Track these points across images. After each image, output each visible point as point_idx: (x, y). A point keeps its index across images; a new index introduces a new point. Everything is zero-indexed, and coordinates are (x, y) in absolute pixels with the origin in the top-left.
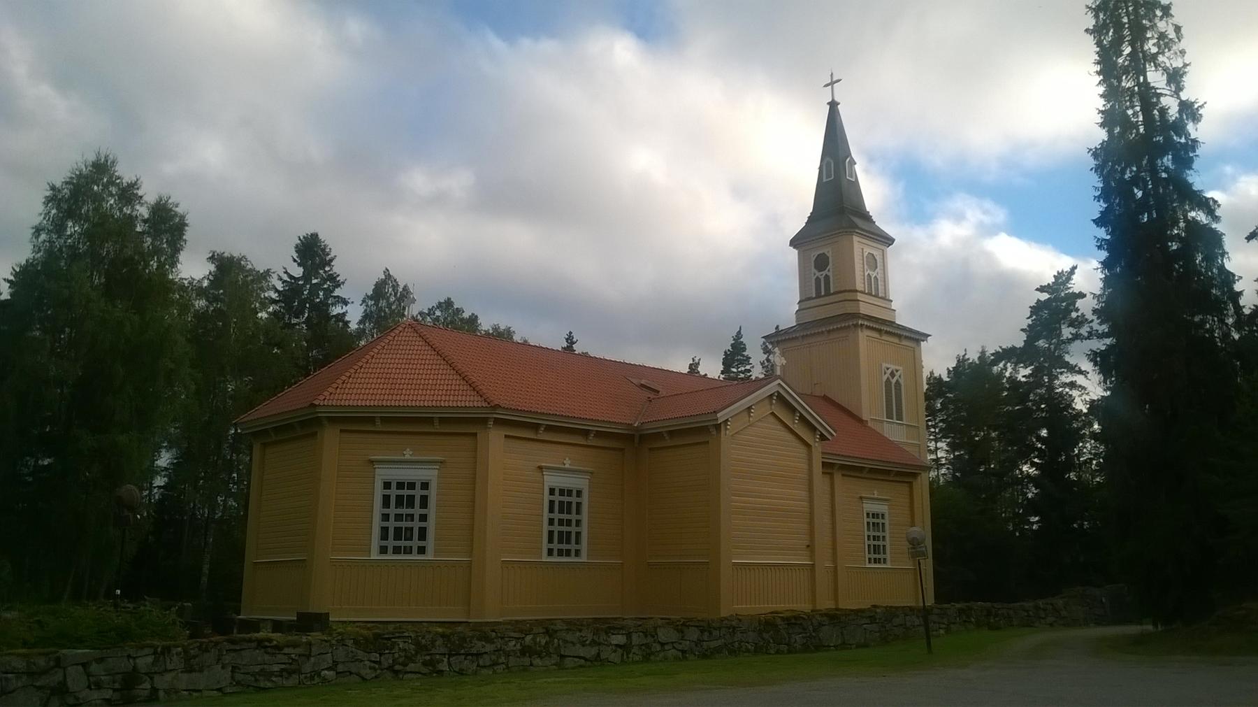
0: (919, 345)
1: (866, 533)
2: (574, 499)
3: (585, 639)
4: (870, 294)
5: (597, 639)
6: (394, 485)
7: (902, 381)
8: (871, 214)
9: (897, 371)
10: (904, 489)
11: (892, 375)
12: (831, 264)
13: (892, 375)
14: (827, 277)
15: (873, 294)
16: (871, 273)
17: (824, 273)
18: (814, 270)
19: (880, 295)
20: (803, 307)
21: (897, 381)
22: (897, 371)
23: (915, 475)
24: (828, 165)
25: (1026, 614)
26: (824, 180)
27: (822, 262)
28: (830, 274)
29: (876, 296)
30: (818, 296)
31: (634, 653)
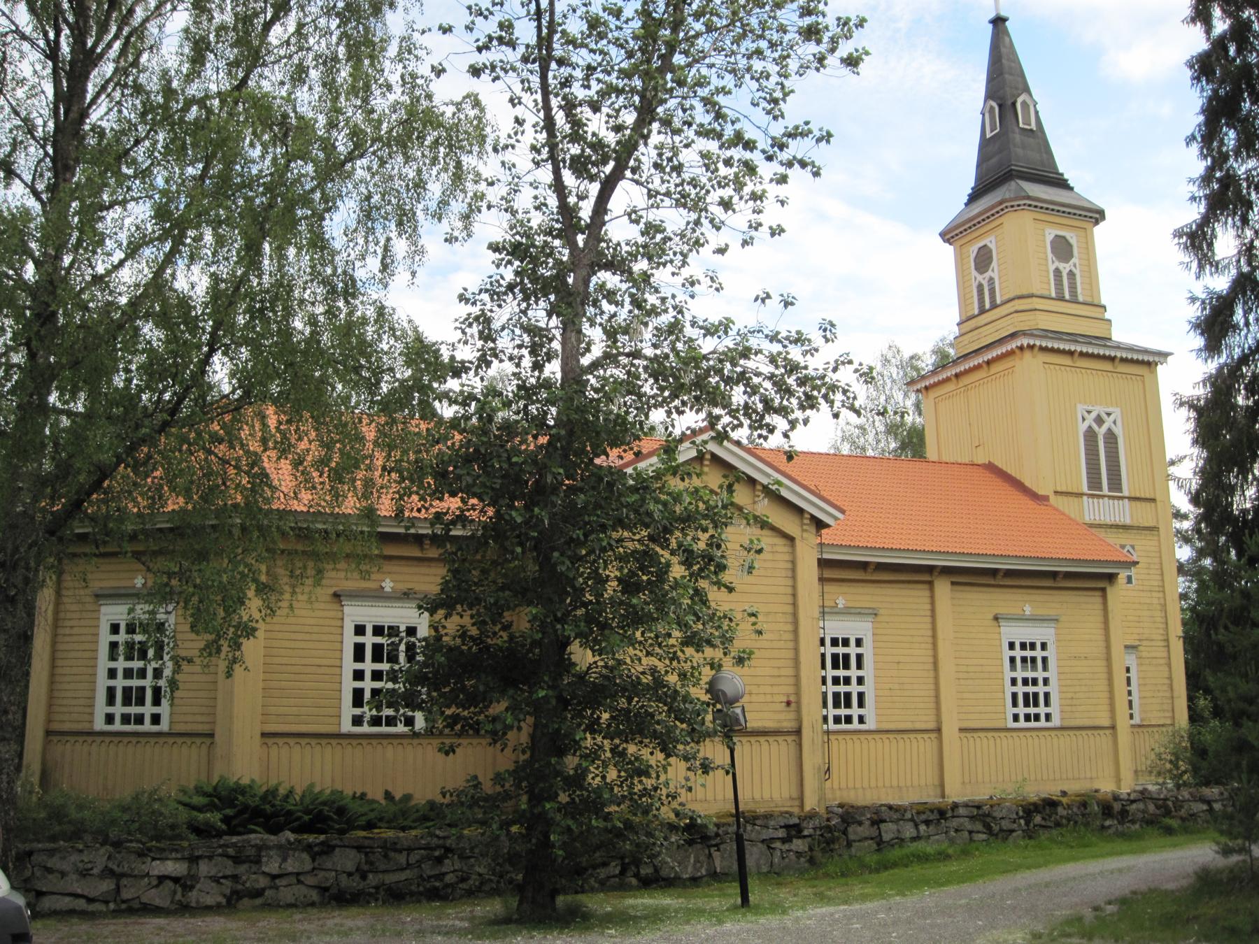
0: (1154, 372)
1: (1009, 675)
2: (1038, 653)
3: (89, 866)
4: (1061, 298)
5: (115, 867)
6: (369, 630)
7: (1118, 431)
8: (1066, 177)
9: (1109, 414)
10: (1096, 599)
11: (1099, 420)
12: (994, 264)
13: (1099, 420)
14: (991, 279)
15: (1067, 296)
16: (1061, 266)
17: (987, 275)
18: (974, 273)
19: (1081, 299)
20: (964, 331)
21: (1109, 430)
22: (1109, 414)
23: (1111, 578)
24: (992, 109)
25: (1205, 807)
26: (988, 136)
27: (983, 260)
28: (995, 276)
29: (1074, 300)
30: (983, 311)
31: (201, 891)
